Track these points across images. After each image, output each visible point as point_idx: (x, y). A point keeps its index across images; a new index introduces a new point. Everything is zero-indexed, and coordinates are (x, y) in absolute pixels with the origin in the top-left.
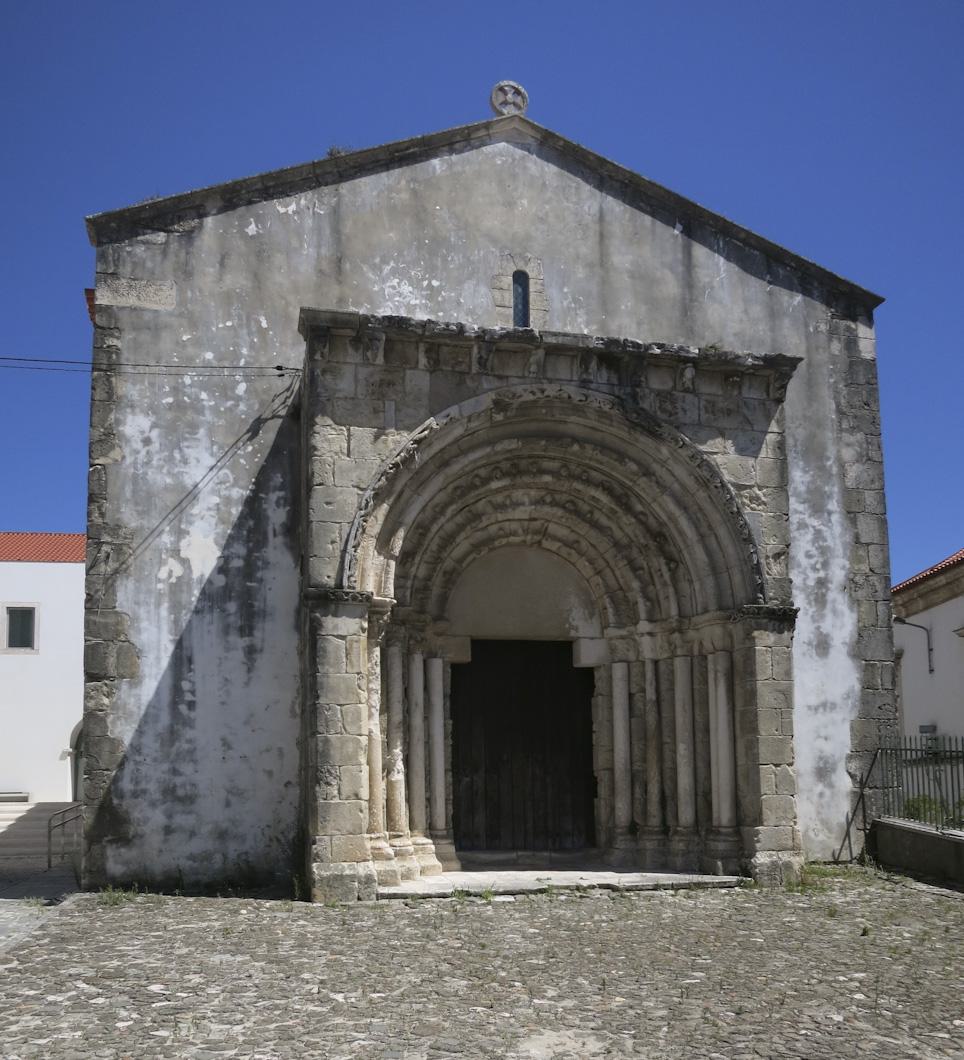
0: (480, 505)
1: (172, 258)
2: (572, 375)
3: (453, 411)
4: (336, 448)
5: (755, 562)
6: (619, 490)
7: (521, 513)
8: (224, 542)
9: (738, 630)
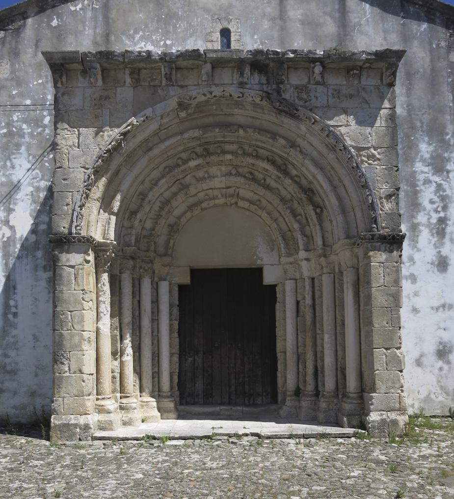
0: (188, 179)
1: (7, 46)
2: (233, 80)
3: (148, 112)
4: (70, 143)
5: (370, 202)
6: (279, 161)
7: (217, 183)
8: (35, 214)
9: (360, 252)
